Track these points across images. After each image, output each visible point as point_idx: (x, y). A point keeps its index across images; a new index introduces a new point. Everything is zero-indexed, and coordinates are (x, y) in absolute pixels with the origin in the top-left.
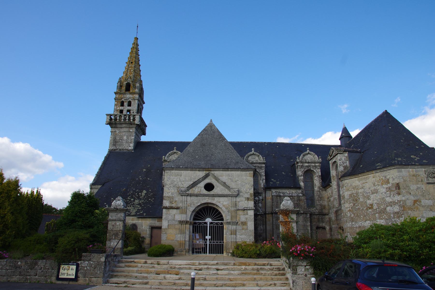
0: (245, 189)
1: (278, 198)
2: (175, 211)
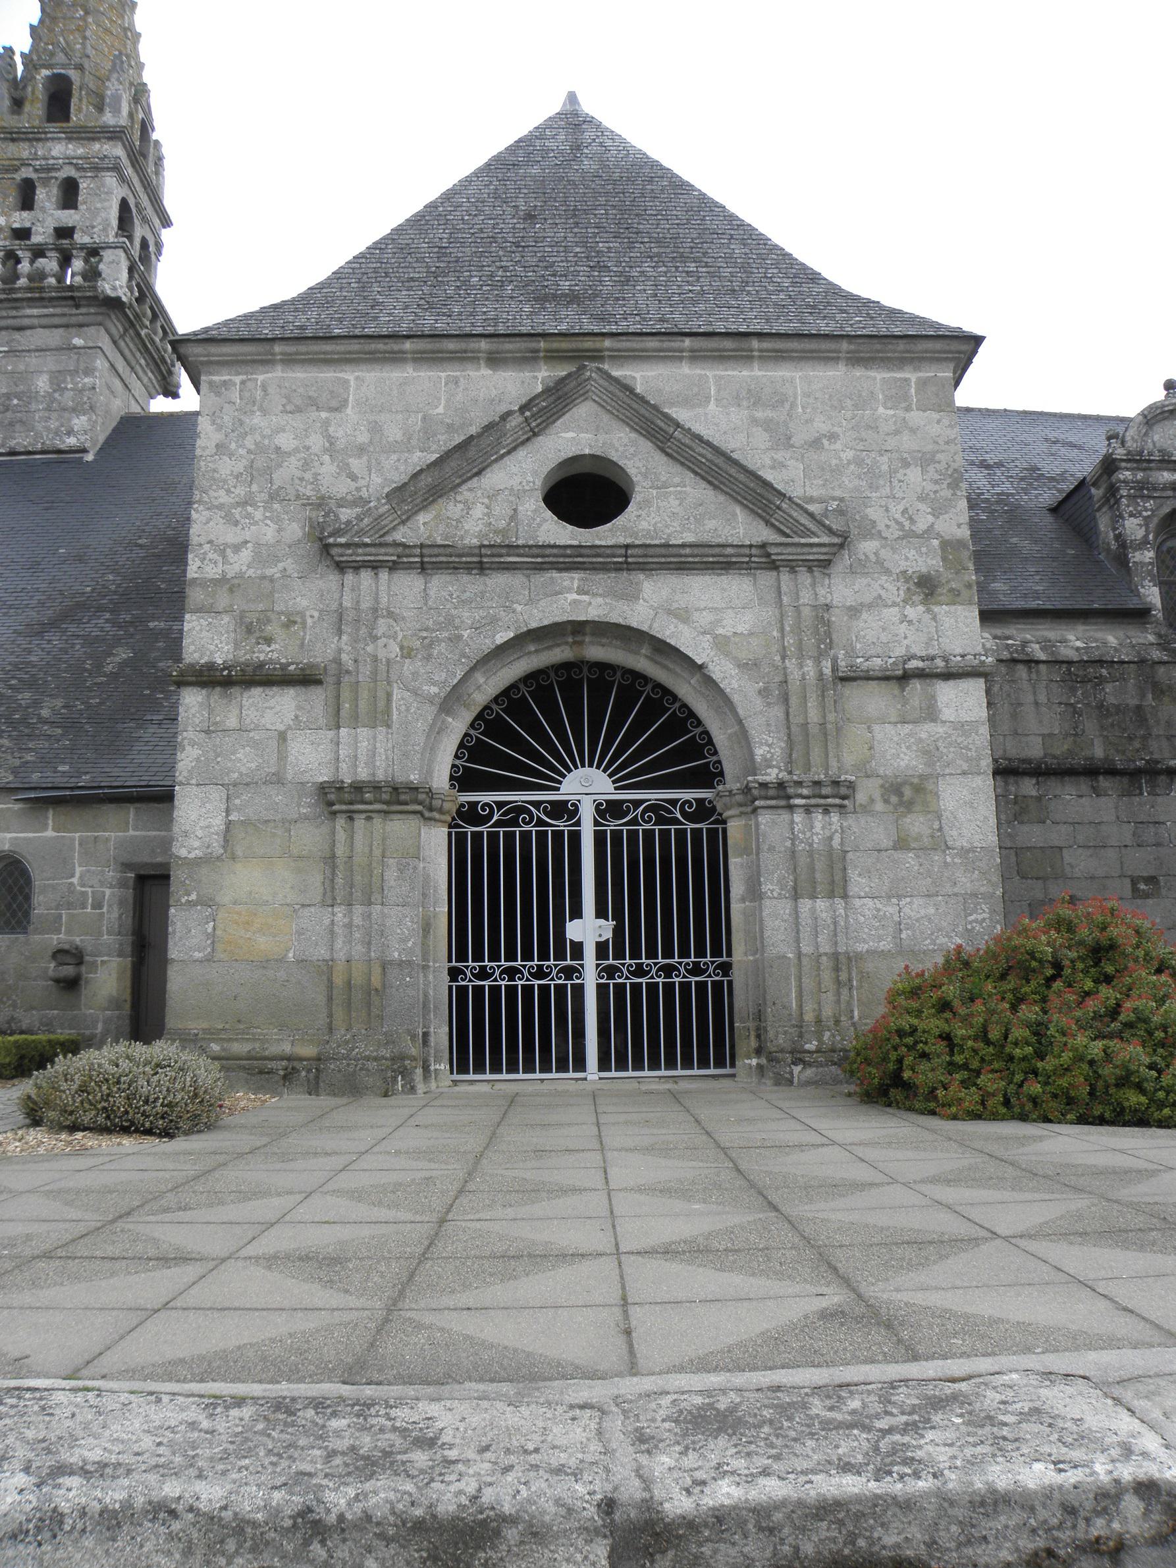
0: (896, 510)
1: (1022, 671)
2: (278, 708)
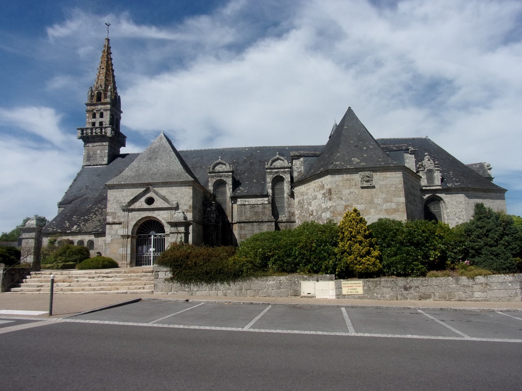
2: (117, 226)
